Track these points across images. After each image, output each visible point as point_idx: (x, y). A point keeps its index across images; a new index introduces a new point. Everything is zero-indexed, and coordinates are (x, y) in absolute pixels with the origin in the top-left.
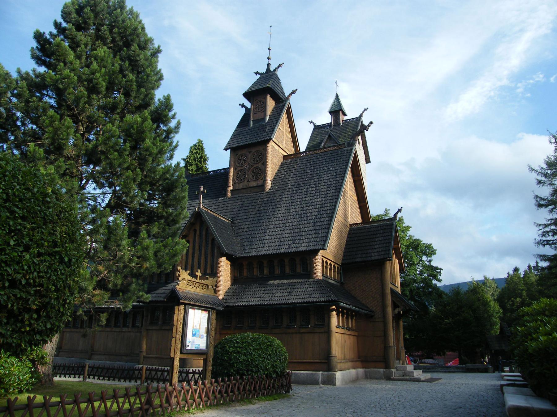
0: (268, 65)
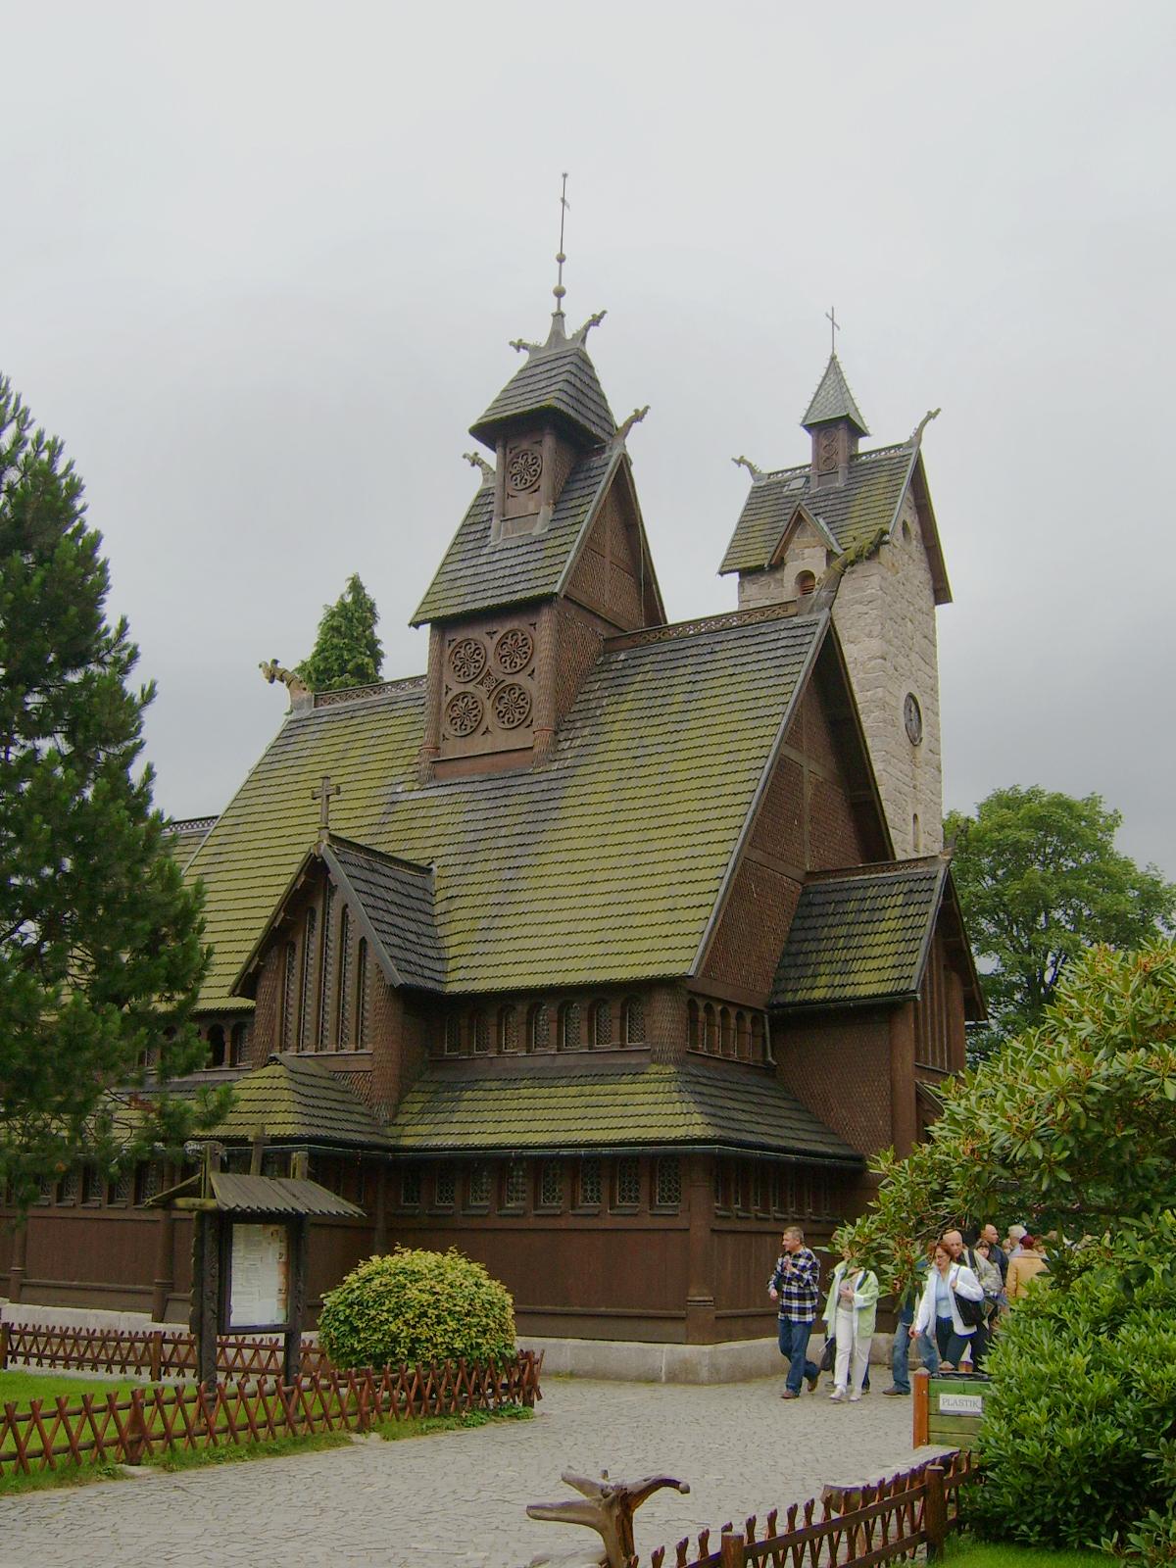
0: (559, 316)
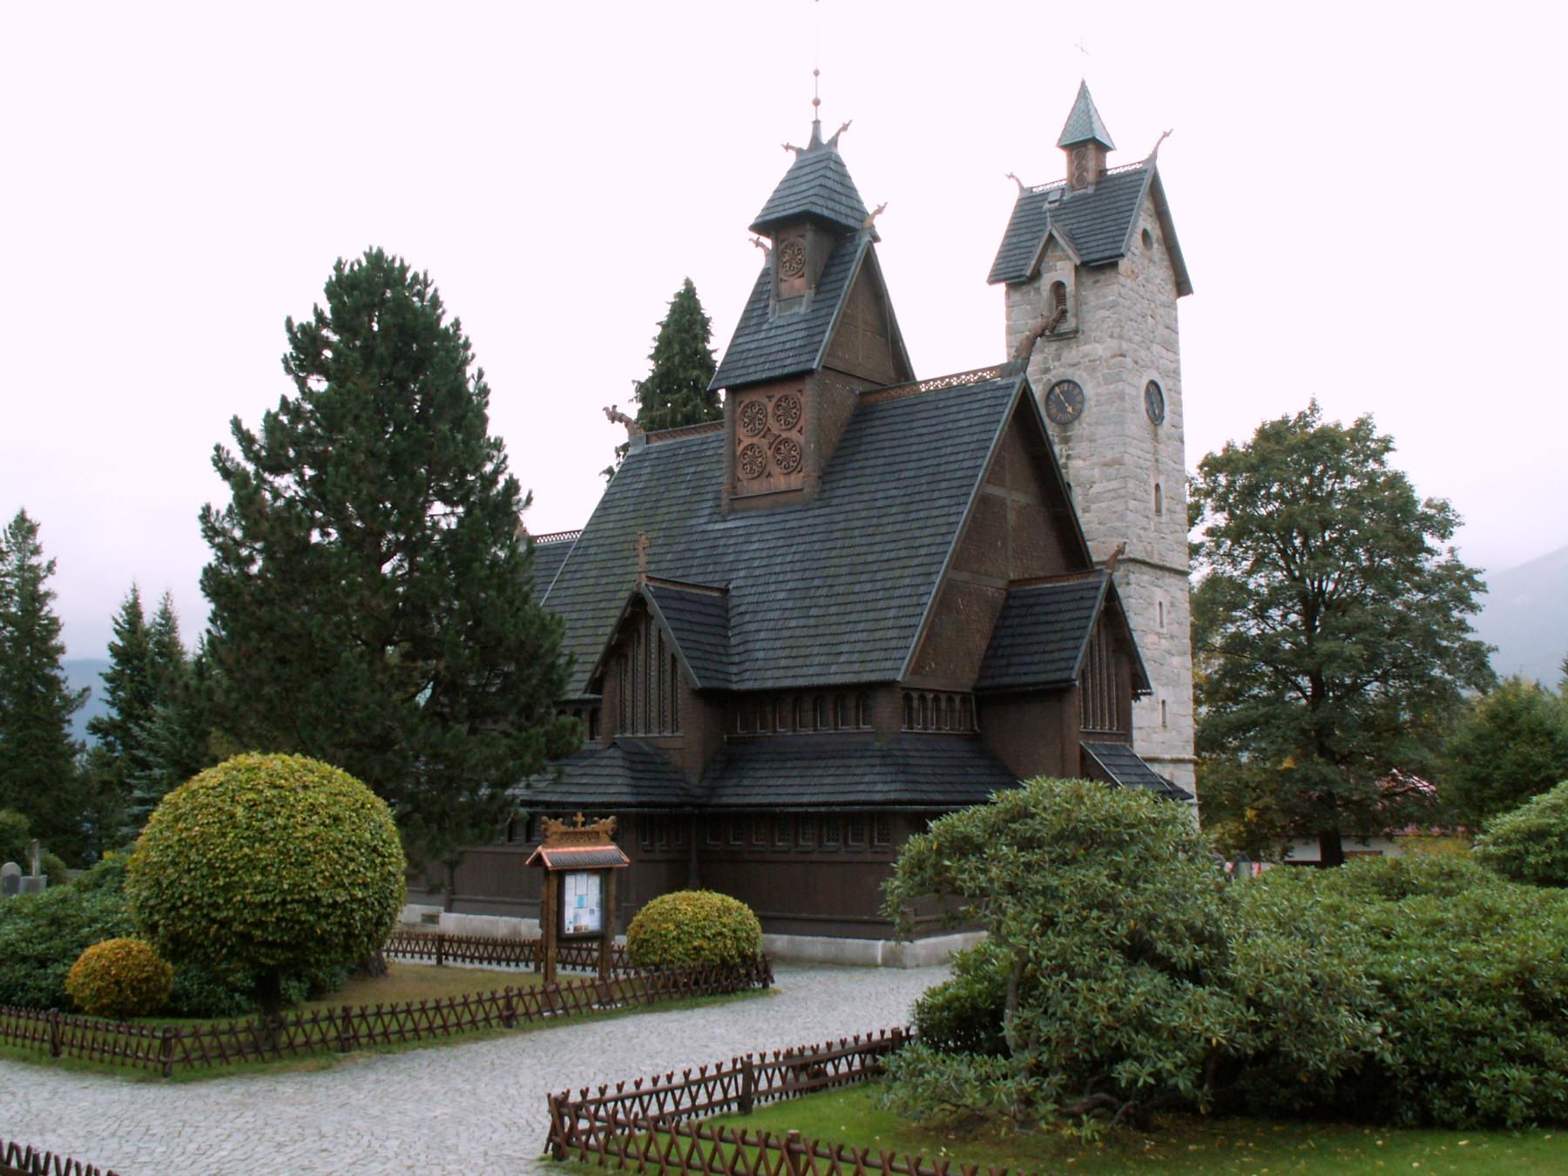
0: (817, 123)
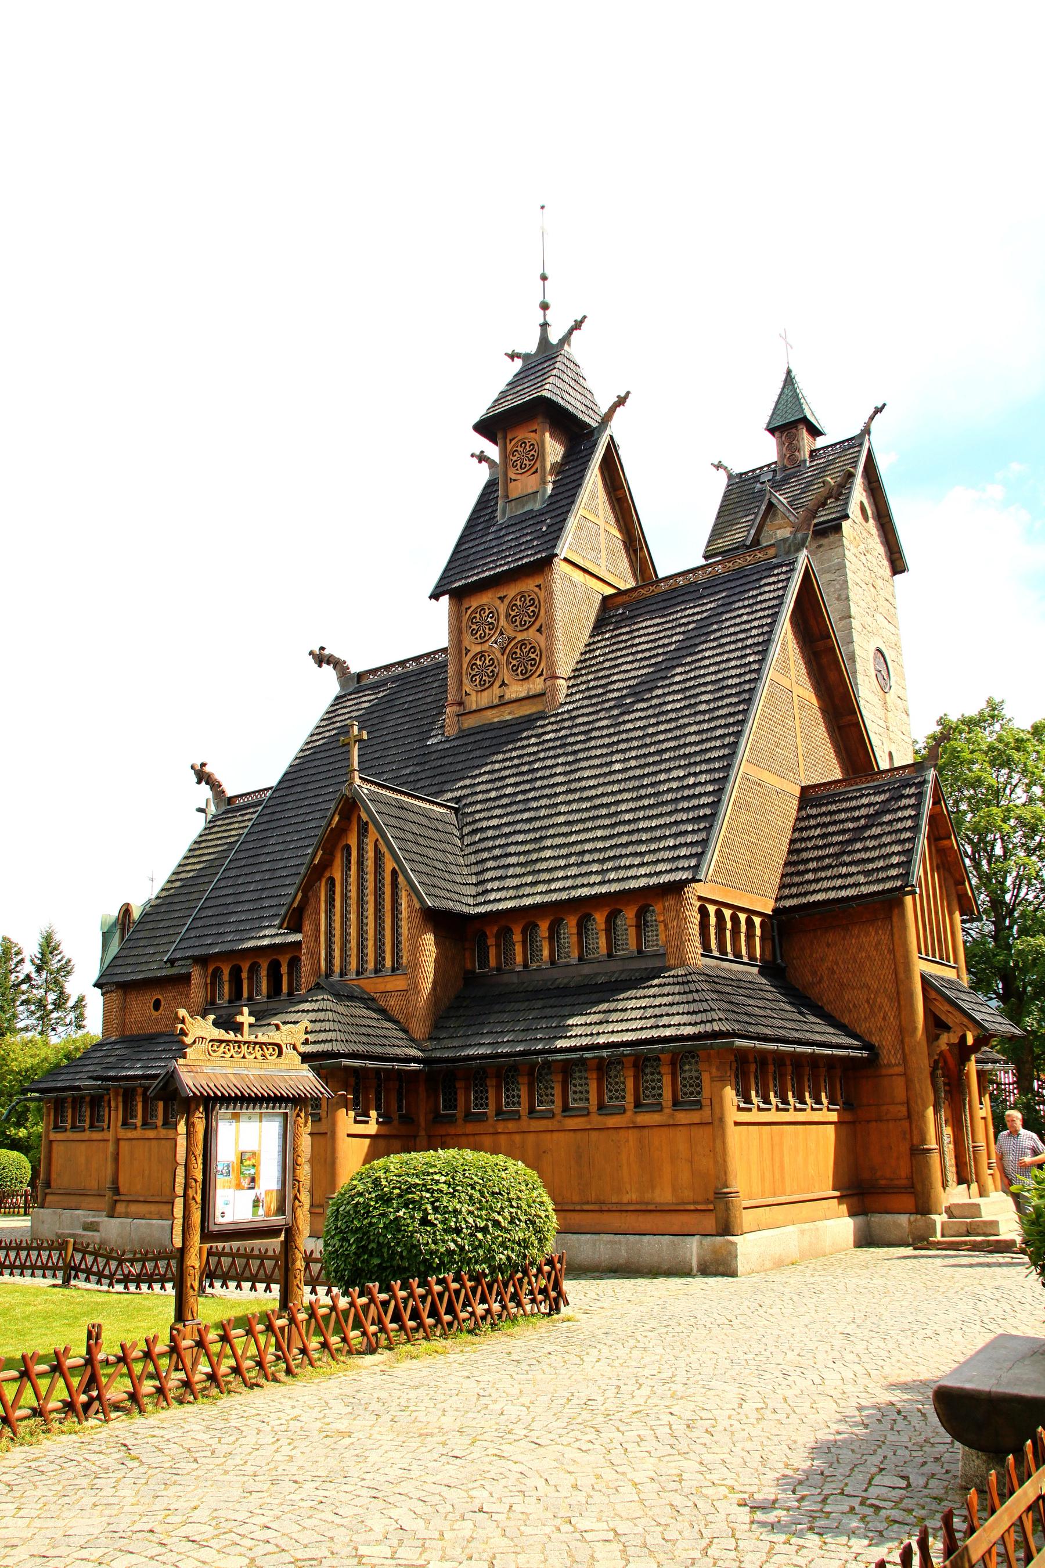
0: (544, 326)
